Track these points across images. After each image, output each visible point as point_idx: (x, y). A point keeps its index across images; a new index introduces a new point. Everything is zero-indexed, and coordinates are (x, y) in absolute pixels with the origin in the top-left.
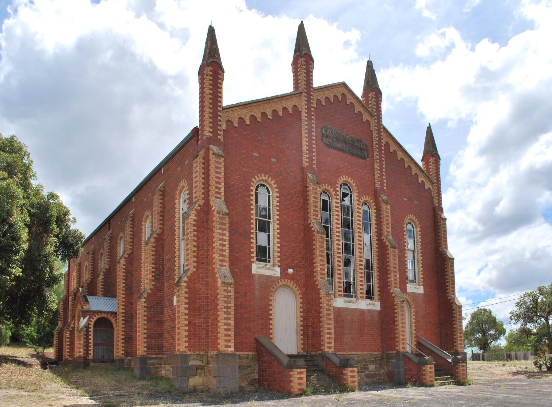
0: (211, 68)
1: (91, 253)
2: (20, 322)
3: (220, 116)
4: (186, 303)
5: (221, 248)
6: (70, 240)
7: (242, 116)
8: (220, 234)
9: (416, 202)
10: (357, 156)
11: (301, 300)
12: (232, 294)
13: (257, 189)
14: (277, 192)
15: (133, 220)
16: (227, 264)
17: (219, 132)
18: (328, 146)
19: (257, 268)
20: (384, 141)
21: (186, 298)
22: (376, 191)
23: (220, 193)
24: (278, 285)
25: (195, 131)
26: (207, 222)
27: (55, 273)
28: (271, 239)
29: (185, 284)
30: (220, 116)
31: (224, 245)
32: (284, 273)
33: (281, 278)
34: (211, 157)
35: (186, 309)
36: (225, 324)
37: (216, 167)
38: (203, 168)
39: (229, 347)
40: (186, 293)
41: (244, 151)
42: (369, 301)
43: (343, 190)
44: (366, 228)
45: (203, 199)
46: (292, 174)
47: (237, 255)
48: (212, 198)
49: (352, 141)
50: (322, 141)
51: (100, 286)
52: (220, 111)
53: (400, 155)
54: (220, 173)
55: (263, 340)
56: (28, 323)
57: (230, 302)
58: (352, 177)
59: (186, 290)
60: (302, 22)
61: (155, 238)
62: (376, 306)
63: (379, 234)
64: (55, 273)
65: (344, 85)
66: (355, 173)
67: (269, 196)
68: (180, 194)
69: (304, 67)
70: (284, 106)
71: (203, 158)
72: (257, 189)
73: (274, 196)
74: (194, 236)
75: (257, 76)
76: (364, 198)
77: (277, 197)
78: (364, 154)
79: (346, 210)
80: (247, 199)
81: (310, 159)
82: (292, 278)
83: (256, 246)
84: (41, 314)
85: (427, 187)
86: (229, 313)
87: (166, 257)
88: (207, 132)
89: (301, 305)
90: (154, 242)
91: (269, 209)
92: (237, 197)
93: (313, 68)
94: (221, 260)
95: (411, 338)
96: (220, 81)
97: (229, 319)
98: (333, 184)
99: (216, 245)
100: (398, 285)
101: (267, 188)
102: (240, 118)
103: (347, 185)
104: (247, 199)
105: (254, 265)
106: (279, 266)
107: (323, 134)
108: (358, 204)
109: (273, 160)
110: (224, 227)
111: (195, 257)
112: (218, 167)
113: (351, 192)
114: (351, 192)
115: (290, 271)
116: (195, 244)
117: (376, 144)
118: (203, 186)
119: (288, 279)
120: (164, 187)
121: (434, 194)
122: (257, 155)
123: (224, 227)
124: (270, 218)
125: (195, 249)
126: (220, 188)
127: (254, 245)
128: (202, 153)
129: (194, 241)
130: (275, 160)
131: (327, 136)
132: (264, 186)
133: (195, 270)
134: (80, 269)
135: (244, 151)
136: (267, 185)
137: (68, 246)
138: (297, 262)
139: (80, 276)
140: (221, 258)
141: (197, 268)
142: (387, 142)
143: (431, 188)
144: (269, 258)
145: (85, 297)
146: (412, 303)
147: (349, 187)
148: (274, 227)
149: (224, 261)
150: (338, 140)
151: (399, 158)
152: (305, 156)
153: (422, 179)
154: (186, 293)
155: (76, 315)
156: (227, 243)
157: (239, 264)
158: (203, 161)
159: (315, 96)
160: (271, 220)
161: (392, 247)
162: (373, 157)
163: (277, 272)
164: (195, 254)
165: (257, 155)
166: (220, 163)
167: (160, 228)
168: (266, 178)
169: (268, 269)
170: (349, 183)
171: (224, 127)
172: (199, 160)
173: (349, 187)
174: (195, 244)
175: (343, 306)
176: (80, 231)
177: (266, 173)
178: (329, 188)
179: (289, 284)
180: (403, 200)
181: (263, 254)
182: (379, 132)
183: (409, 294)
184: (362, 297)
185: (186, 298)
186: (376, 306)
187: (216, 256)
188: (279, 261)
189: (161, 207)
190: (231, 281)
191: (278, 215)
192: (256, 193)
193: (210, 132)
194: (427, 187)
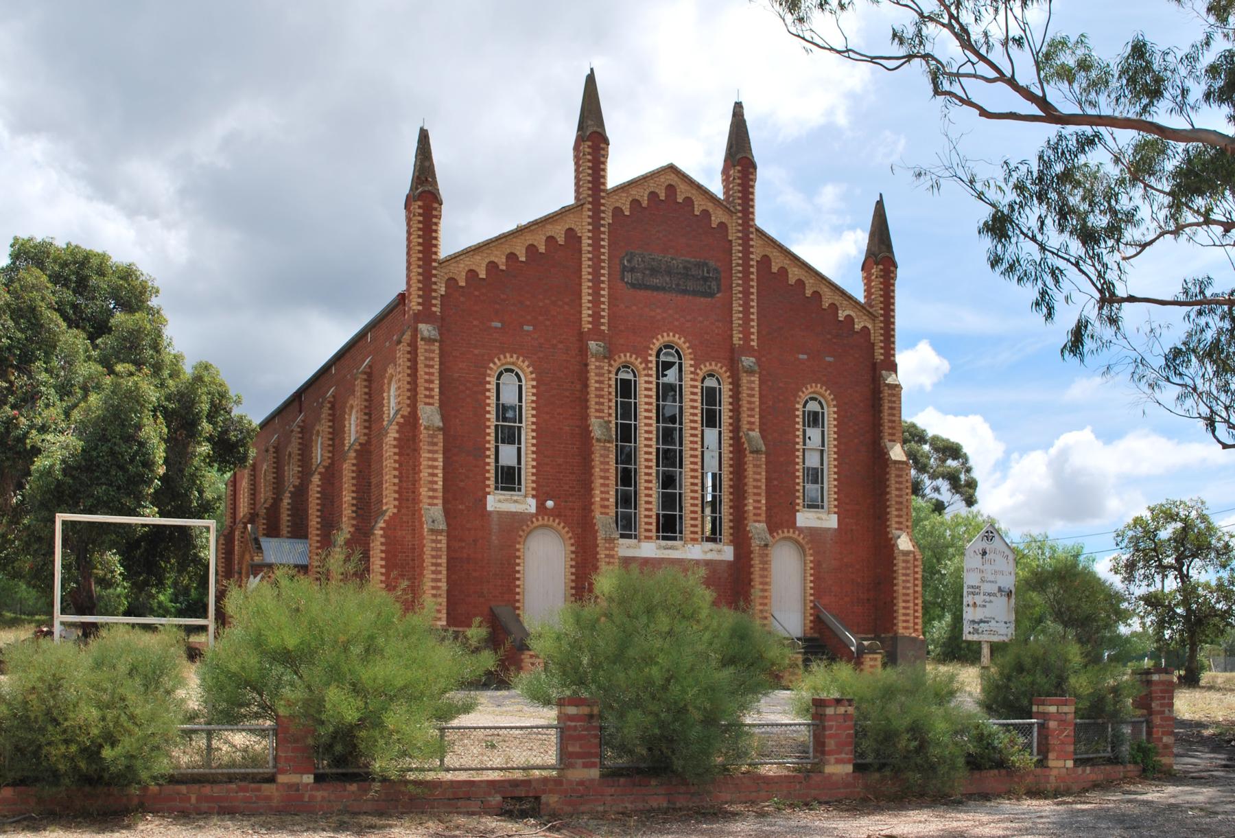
0: (420, 203)
1: (272, 450)
2: (147, 583)
3: (435, 276)
4: (382, 559)
5: (430, 478)
6: (232, 436)
7: (474, 267)
8: (430, 459)
9: (828, 359)
10: (695, 293)
11: (573, 549)
12: (443, 545)
13: (498, 378)
14: (533, 380)
15: (332, 408)
16: (440, 501)
17: (434, 302)
18: (633, 286)
19: (496, 502)
20: (755, 257)
21: (382, 551)
22: (732, 349)
23: (432, 397)
24: (532, 526)
25: (402, 297)
26: (414, 440)
27: (208, 495)
28: (521, 454)
29: (381, 532)
30: (435, 276)
31: (436, 475)
32: (541, 507)
33: (537, 514)
34: (420, 343)
35: (382, 566)
36: (433, 588)
37: (426, 359)
38: (409, 360)
39: (440, 619)
40: (382, 544)
41: (475, 323)
42: (710, 545)
43: (663, 358)
44: (711, 419)
45: (408, 406)
46: (560, 346)
47: (462, 484)
48: (421, 406)
49: (685, 268)
50: (622, 279)
51: (285, 517)
52: (435, 268)
53: (794, 274)
54: (432, 367)
55: (502, 611)
56: (160, 584)
57: (440, 557)
58: (681, 331)
59: (383, 540)
60: (592, 70)
61: (356, 451)
62: (727, 553)
63: (736, 428)
64: (208, 495)
65: (672, 168)
66: (688, 324)
67: (520, 387)
68: (389, 384)
69: (589, 157)
70: (549, 234)
71: (409, 345)
72: (498, 378)
73: (528, 385)
74: (395, 461)
75: (509, 185)
76: (706, 367)
77: (533, 387)
78: (710, 287)
79: (667, 392)
80: (480, 397)
81: (596, 316)
82: (556, 513)
83: (497, 467)
84: (182, 569)
85: (858, 327)
86: (440, 572)
87: (374, 481)
88: (414, 305)
89: (573, 556)
90: (356, 458)
91: (520, 407)
92: (460, 397)
93: (606, 156)
94: (430, 497)
95: (805, 610)
96: (434, 220)
97: (439, 580)
98: (642, 352)
99: (424, 474)
100: (763, 517)
101: (517, 375)
102: (471, 271)
103: (672, 348)
104: (480, 397)
105: (490, 498)
106: (533, 496)
107: (625, 267)
108: (692, 380)
109: (526, 328)
110: (436, 448)
111: (395, 492)
112: (430, 357)
113: (680, 358)
114: (680, 358)
115: (550, 504)
116: (397, 473)
117: (738, 265)
118: (408, 387)
119: (549, 516)
120: (370, 367)
121: (877, 337)
122: (499, 325)
123: (436, 448)
124: (520, 422)
125: (396, 481)
126: (431, 390)
127: (492, 468)
128: (407, 337)
129: (395, 469)
130: (531, 328)
131: (632, 270)
132: (512, 371)
133: (395, 511)
134: (254, 476)
135: (475, 323)
136: (517, 370)
137: (227, 450)
138: (566, 487)
139: (254, 489)
140: (431, 494)
141: (399, 508)
142: (766, 256)
143: (870, 327)
144: (520, 483)
145: (257, 541)
146: (807, 547)
147: (677, 351)
148: (528, 437)
149: (435, 498)
150: (654, 272)
151: (792, 281)
152: (586, 313)
153: (847, 313)
154: (382, 544)
155: (244, 572)
156: (440, 472)
157: (461, 496)
158: (409, 349)
159: (608, 206)
160: (523, 425)
161: (752, 452)
162: (731, 288)
163: (531, 505)
164: (396, 488)
165: (499, 325)
166: (433, 351)
167: (365, 434)
168: (514, 359)
169: (516, 501)
170: (677, 344)
171: (443, 291)
172: (403, 348)
173: (677, 351)
174: (397, 473)
175: (653, 556)
176: (248, 418)
177: (512, 352)
178: (633, 360)
179: (551, 522)
180: (798, 359)
181: (509, 478)
182: (746, 240)
183: (801, 530)
184: (693, 540)
185: (382, 551)
186: (727, 553)
187: (424, 491)
188: (533, 489)
189: (366, 400)
190: (443, 526)
191: (533, 416)
192: (498, 385)
193: (419, 304)
194: (858, 327)
